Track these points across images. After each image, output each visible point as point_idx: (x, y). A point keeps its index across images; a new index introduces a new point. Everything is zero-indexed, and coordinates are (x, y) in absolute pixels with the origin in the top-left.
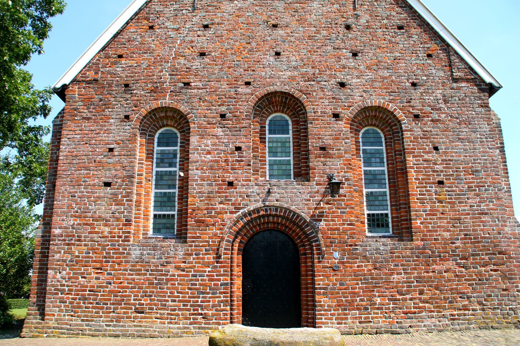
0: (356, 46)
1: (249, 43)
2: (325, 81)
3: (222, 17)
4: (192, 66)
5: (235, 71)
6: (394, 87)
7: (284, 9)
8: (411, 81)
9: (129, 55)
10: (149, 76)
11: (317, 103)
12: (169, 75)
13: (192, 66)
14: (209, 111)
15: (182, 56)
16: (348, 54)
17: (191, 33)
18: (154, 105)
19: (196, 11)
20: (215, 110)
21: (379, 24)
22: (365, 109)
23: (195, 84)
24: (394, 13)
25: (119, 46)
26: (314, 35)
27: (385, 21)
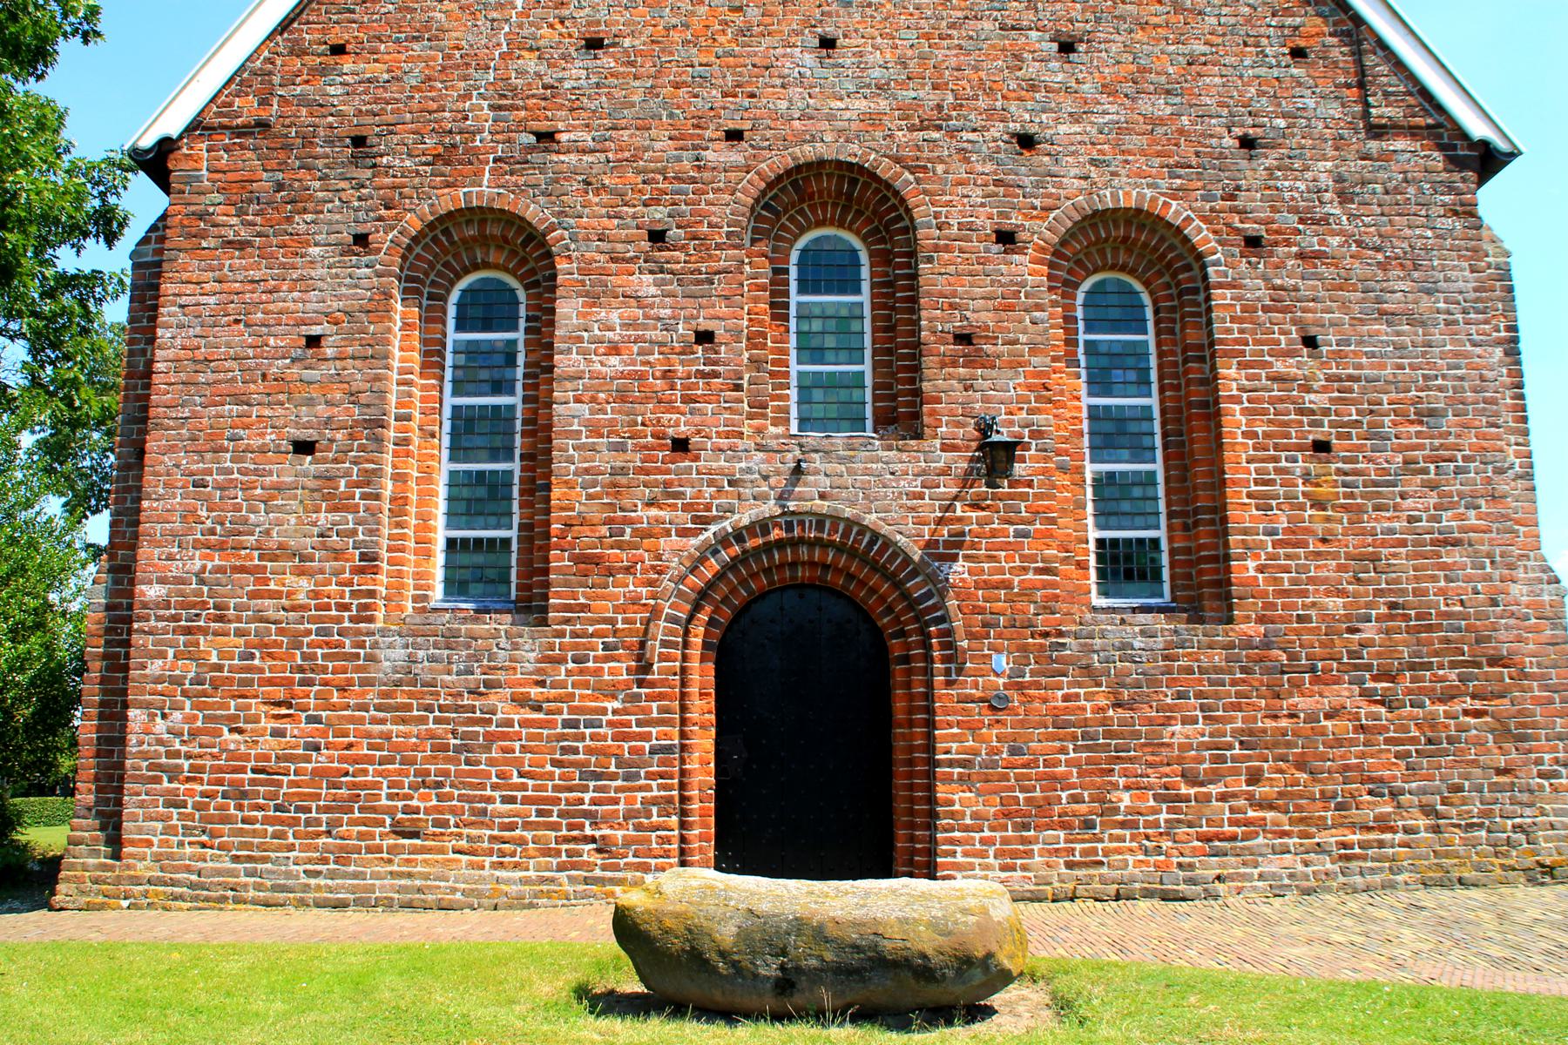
0: (1071, 21)
2: (974, 130)
5: (696, 96)
6: (1187, 151)
9: (367, 45)
10: (430, 113)
11: (948, 198)
13: (561, 80)
14: (616, 222)
15: (531, 49)
18: (448, 200)
20: (634, 217)
22: (1096, 220)
25: (335, 18)
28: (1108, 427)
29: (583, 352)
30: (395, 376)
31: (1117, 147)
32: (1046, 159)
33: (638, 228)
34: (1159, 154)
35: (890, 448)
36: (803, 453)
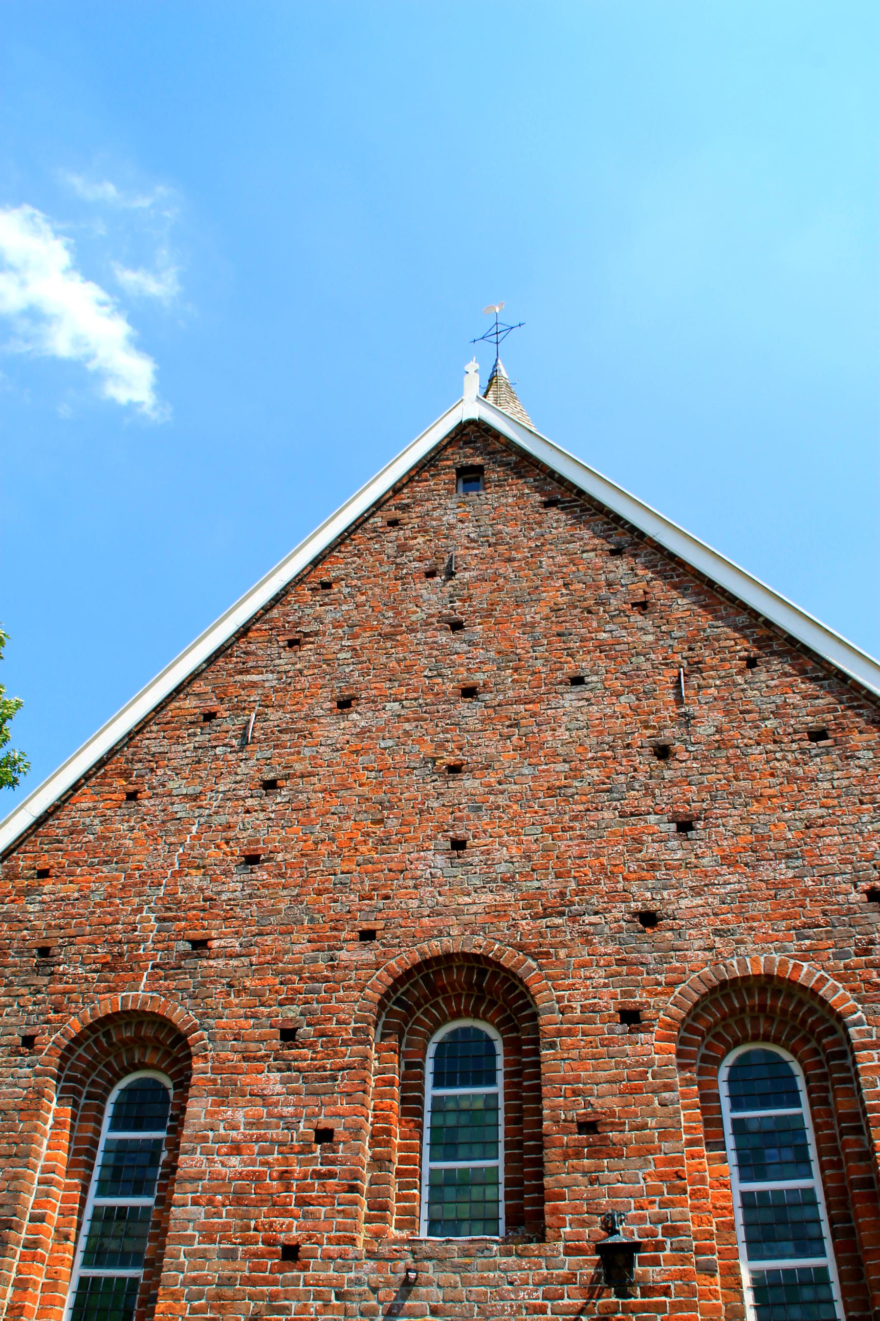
0: (687, 802)
1: (380, 821)
2: (596, 913)
3: (315, 758)
4: (219, 893)
5: (336, 901)
6: (813, 911)
7: (482, 722)
8: (864, 885)
9: (67, 869)
10: (106, 925)
11: (571, 981)
12: (158, 919)
13: (219, 893)
14: (252, 1021)
15: (198, 868)
16: (664, 827)
17: (229, 804)
18: (106, 1005)
19: (249, 748)
20: (269, 1016)
21: (752, 733)
22: (724, 990)
23: (222, 943)
24: (795, 699)
25: (46, 847)
26: (564, 782)
27: (770, 724)
28: (766, 1216)
29: (206, 1152)
30: (37, 1175)
31: (740, 914)
32: (669, 934)
33: (272, 1027)
34: (784, 918)
35: (508, 1254)
36: (416, 1261)
